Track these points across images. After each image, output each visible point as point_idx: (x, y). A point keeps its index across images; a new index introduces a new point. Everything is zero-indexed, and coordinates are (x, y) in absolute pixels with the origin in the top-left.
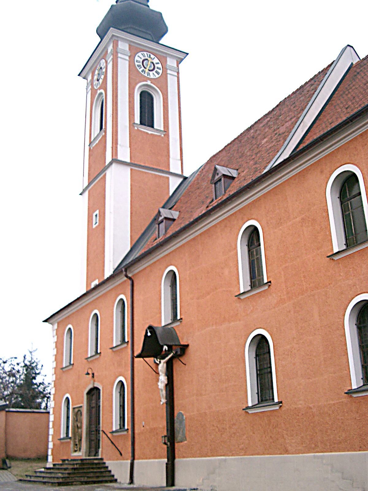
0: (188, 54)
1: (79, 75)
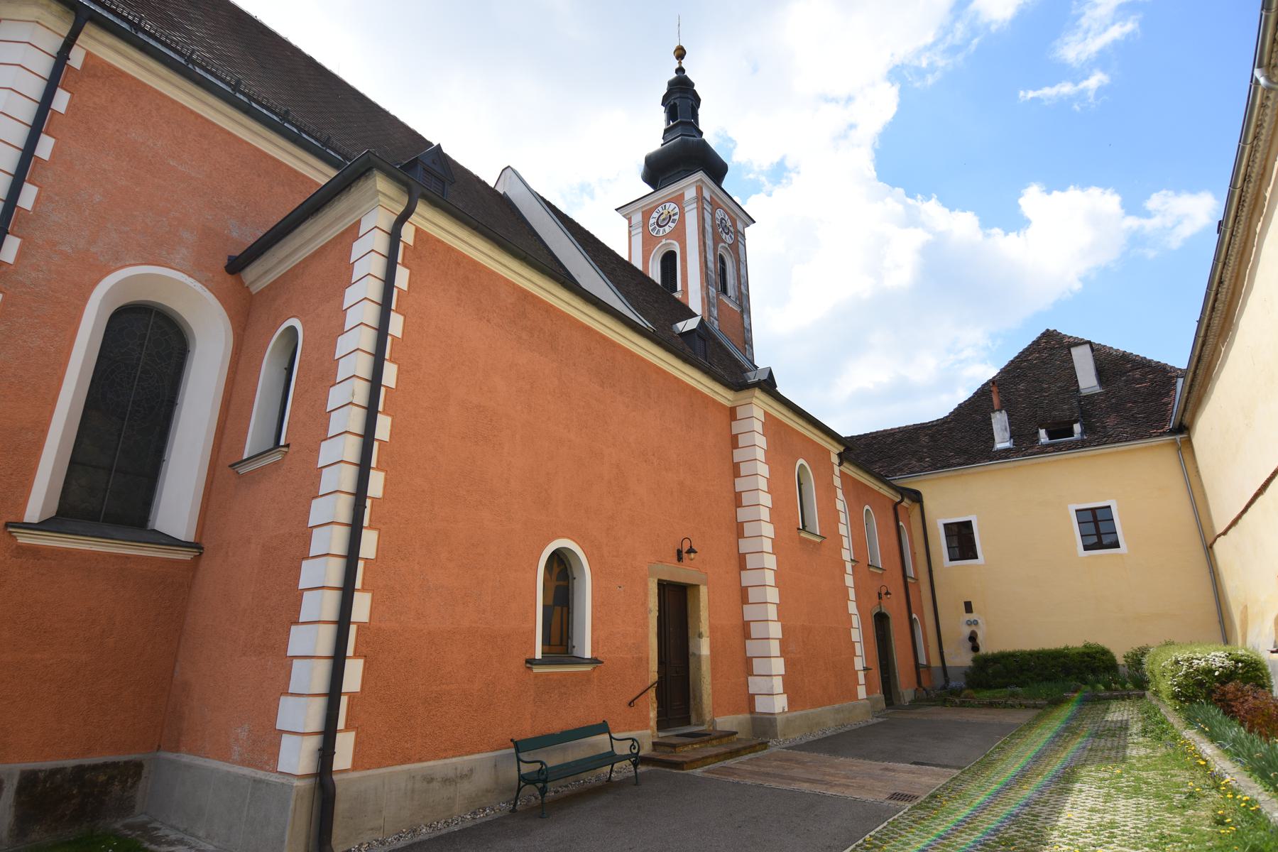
0: (754, 222)
1: (617, 210)
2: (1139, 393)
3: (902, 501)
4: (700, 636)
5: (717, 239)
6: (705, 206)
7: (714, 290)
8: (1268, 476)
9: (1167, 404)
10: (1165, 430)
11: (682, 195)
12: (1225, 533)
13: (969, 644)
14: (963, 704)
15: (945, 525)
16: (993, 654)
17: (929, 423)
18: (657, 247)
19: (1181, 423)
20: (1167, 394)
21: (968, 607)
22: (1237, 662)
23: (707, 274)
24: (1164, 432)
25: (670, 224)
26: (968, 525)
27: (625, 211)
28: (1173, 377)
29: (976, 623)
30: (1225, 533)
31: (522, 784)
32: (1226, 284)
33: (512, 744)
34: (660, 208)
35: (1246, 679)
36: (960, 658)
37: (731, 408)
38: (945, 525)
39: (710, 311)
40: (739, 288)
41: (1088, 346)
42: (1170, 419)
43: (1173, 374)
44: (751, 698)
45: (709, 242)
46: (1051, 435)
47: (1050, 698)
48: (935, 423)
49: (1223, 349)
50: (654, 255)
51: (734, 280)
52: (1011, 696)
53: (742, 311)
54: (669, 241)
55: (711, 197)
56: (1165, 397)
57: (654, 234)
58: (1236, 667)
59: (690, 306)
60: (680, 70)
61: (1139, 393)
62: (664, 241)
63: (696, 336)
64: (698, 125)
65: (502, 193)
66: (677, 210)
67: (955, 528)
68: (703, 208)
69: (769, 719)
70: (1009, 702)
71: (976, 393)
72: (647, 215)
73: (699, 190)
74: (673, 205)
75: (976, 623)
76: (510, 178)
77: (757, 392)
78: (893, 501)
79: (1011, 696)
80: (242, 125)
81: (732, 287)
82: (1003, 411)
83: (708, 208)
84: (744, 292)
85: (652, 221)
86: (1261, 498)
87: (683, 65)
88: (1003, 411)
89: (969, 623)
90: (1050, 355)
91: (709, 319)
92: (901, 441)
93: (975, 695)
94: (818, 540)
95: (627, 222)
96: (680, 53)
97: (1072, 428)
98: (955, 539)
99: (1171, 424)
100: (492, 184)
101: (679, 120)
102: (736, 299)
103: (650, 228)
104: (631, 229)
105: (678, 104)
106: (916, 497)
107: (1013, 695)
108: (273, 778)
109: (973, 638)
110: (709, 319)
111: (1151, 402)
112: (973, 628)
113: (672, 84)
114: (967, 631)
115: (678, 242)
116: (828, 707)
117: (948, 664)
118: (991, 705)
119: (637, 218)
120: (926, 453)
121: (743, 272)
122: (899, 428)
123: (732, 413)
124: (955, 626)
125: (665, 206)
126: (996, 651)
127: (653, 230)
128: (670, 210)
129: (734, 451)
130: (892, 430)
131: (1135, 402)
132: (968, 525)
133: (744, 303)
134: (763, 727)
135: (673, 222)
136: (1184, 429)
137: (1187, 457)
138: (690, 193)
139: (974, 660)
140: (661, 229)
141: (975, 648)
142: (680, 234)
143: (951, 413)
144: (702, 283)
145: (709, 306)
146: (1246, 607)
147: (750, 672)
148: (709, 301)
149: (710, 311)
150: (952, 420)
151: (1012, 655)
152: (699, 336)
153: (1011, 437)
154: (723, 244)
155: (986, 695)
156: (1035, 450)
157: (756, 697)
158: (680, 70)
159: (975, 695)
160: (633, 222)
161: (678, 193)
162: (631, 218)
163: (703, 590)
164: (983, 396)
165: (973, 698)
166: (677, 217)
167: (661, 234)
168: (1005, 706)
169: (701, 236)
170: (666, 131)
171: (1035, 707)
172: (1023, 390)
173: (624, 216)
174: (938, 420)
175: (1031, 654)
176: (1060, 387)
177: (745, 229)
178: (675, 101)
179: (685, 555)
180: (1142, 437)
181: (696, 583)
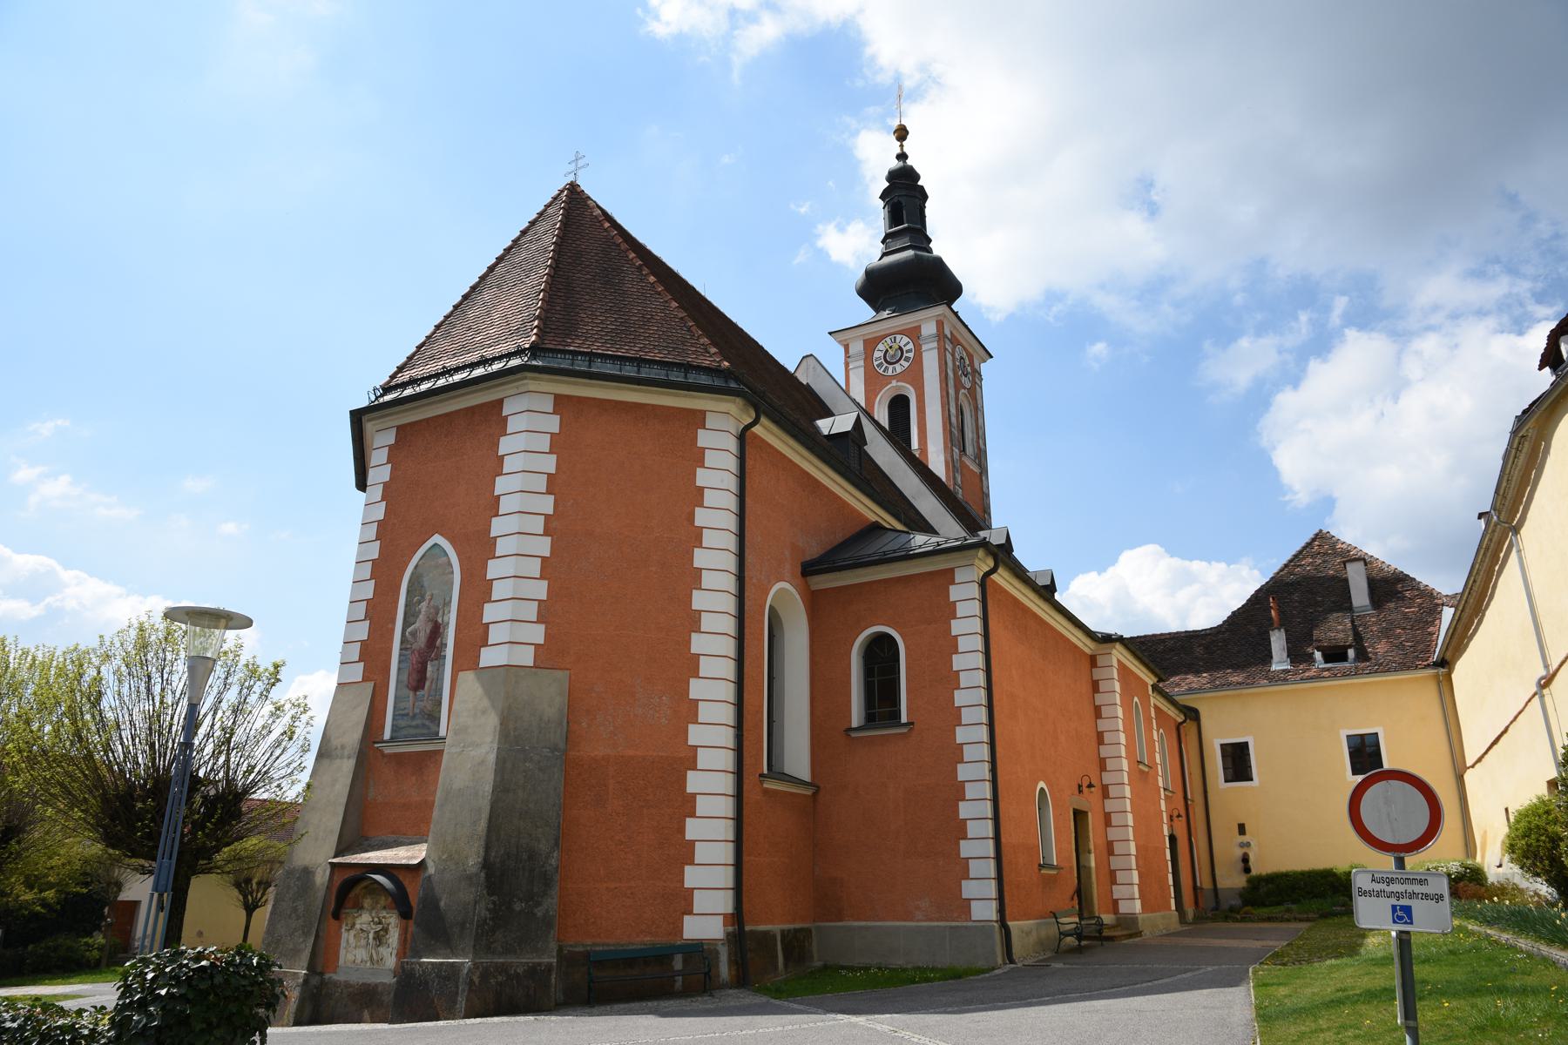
0: (992, 357)
1: (830, 333)
2: (1407, 618)
3: (1184, 721)
4: (1089, 852)
5: (958, 386)
6: (947, 346)
7: (957, 451)
8: (1499, 733)
9: (1431, 634)
10: (1428, 662)
11: (918, 328)
12: (1473, 766)
13: (1241, 865)
14: (1243, 920)
15: (1222, 745)
16: (1267, 875)
17: (1202, 630)
18: (883, 391)
19: (1443, 658)
20: (1432, 623)
21: (1242, 829)
22: (1466, 868)
23: (951, 432)
24: (1429, 665)
25: (902, 362)
26: (1244, 746)
27: (842, 336)
28: (1438, 605)
29: (1248, 845)
30: (1473, 766)
31: (1062, 937)
32: (1478, 583)
33: (1052, 915)
34: (888, 339)
35: (1471, 880)
36: (1231, 880)
37: (1091, 656)
38: (1222, 745)
39: (955, 478)
40: (978, 442)
41: (1362, 563)
42: (1435, 651)
43: (1440, 602)
44: (1115, 903)
45: (952, 392)
46: (1327, 659)
47: (1320, 912)
48: (1208, 632)
49: (1476, 621)
50: (881, 397)
51: (973, 433)
52: (1286, 911)
53: (981, 473)
54: (900, 384)
55: (951, 333)
56: (1431, 626)
57: (881, 372)
58: (1465, 872)
59: (931, 467)
60: (902, 156)
61: (1407, 618)
62: (894, 383)
63: (850, 441)
64: (926, 230)
65: (805, 383)
66: (911, 346)
67: (1229, 749)
68: (946, 349)
69: (1131, 918)
70: (1286, 917)
71: (1249, 600)
72: (870, 345)
73: (940, 325)
74: (906, 340)
75: (1248, 845)
76: (814, 368)
77: (1118, 646)
78: (1175, 720)
79: (1286, 911)
80: (799, 454)
81: (970, 441)
82: (1282, 630)
83: (949, 347)
84: (982, 447)
85: (877, 354)
86: (1495, 747)
87: (905, 150)
88: (1282, 630)
89: (1242, 845)
90: (1324, 562)
91: (954, 488)
92: (1173, 651)
93: (1254, 912)
94: (1146, 769)
95: (842, 350)
96: (902, 134)
97: (1346, 653)
98: (1230, 759)
99: (1435, 657)
100: (791, 369)
101: (906, 225)
102: (975, 458)
103: (876, 363)
104: (849, 360)
105: (904, 204)
106: (1192, 714)
107: (1288, 910)
108: (970, 924)
109: (1245, 859)
110: (954, 488)
111: (1418, 629)
112: (1245, 850)
113: (893, 176)
114: (1239, 852)
115: (911, 385)
116: (1158, 914)
117: (1219, 886)
118: (1269, 919)
119: (857, 347)
120: (1202, 667)
121: (980, 421)
122: (1170, 634)
123: (1093, 661)
124: (1227, 847)
125: (895, 338)
126: (1269, 871)
127: (880, 365)
128: (902, 344)
129: (1096, 695)
130: (1162, 635)
131: (1404, 629)
132: (1244, 746)
133: (983, 460)
134: (1128, 925)
135: (907, 359)
136: (1445, 665)
137: (1445, 689)
138: (929, 329)
139: (1249, 881)
140: (891, 367)
141: (1247, 870)
142: (915, 374)
143: (1224, 622)
144: (945, 443)
145: (954, 472)
146: (1485, 832)
147: (1113, 881)
148: (954, 466)
149: (955, 478)
150: (1227, 630)
151: (1285, 876)
152: (853, 441)
153: (1288, 656)
154: (963, 391)
155: (1264, 911)
156: (1311, 673)
157: (1120, 901)
158: (902, 156)
159: (1254, 912)
160: (851, 351)
161: (914, 325)
162: (848, 345)
163: (1090, 814)
164: (1258, 604)
165: (1252, 914)
166: (911, 355)
167: (890, 373)
168: (1282, 920)
169: (944, 385)
170: (887, 236)
171: (1308, 920)
172: (1296, 601)
173: (840, 342)
174: (1211, 628)
175: (1303, 873)
176: (1333, 602)
177: (982, 365)
178: (900, 199)
179: (1085, 790)
180: (1408, 668)
181: (1086, 810)
